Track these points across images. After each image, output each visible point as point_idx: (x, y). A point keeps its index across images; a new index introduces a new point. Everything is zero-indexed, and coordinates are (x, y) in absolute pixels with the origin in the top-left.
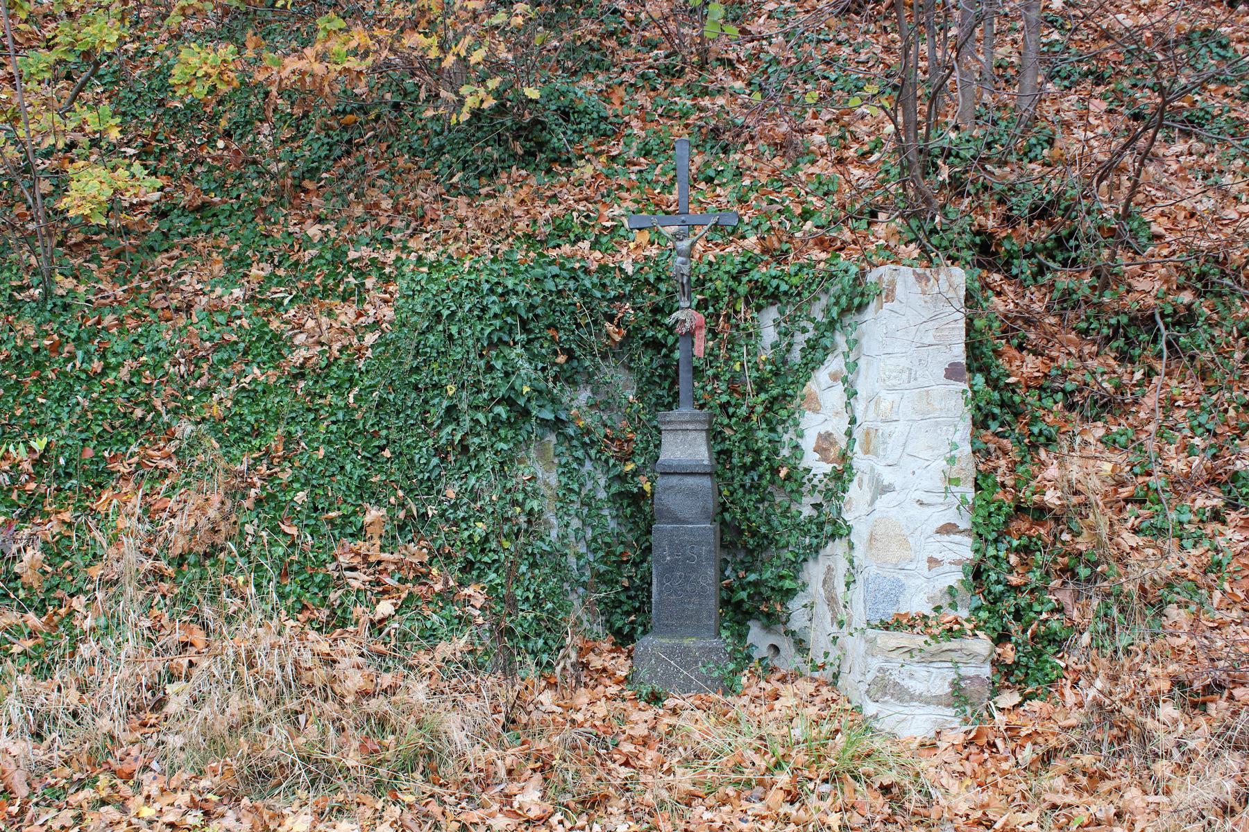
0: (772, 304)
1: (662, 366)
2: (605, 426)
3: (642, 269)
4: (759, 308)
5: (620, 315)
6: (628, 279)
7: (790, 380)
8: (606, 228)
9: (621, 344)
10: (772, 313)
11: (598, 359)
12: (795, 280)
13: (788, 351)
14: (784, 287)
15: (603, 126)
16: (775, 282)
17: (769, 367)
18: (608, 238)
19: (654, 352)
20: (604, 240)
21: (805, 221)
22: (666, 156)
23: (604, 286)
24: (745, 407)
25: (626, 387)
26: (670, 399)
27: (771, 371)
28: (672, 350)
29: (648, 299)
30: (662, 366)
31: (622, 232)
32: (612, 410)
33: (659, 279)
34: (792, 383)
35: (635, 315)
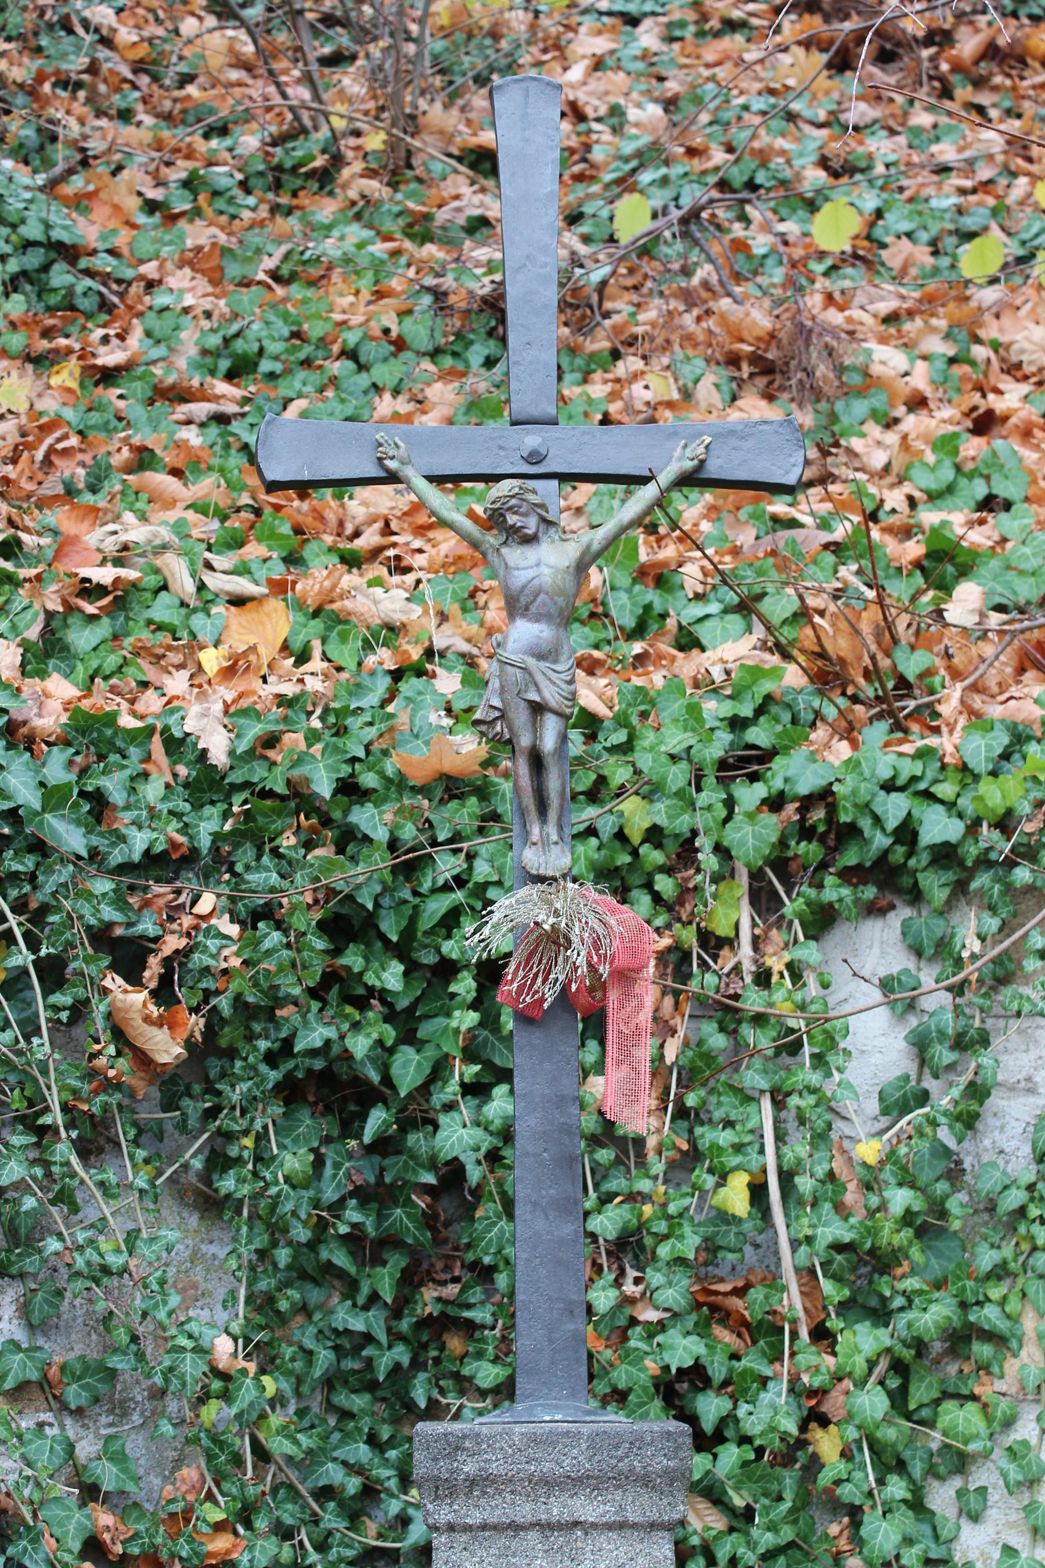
0: (875, 910)
1: (363, 1195)
2: (91, 1493)
3: (271, 741)
4: (822, 921)
5: (173, 943)
6: (206, 784)
7: (986, 1259)
8: (89, 590)
9: (172, 1086)
10: (878, 946)
11: (63, 1151)
12: (994, 795)
13: (968, 1121)
14: (938, 827)
15: (60, 276)
16: (894, 808)
17: (900, 1199)
18: (104, 629)
19: (328, 1125)
20: (82, 638)
21: (945, 588)
22: (316, 377)
23: (98, 801)
24: (777, 1394)
25: (193, 1295)
26: (401, 1354)
27: (908, 1218)
28: (418, 1115)
29: (302, 877)
30: (363, 1195)
31: (163, 609)
32: (121, 1409)
33: (349, 790)
34: (1000, 1273)
35: (249, 941)
